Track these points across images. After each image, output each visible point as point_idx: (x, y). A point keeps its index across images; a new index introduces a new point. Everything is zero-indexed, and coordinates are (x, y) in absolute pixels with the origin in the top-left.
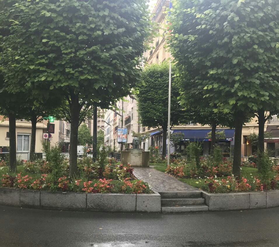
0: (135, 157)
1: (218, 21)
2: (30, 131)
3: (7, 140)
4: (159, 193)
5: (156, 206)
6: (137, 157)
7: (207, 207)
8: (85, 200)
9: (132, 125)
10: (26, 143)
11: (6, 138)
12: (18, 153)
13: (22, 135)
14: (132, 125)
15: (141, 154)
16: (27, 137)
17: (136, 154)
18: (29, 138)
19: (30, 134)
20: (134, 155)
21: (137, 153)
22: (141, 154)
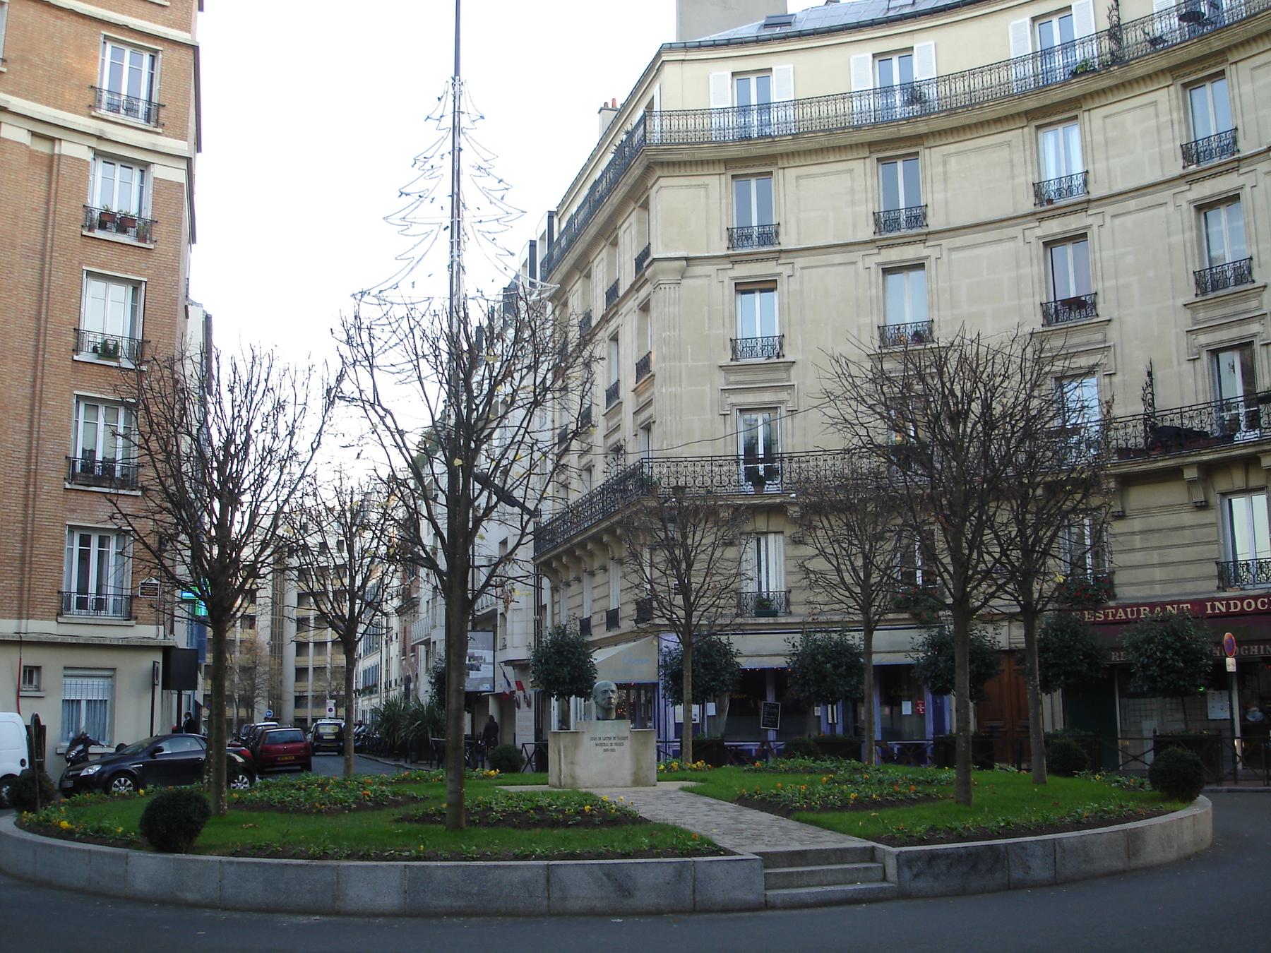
0: (606, 750)
6: (613, 750)
12: (1209, 578)
20: (601, 745)
21: (610, 738)
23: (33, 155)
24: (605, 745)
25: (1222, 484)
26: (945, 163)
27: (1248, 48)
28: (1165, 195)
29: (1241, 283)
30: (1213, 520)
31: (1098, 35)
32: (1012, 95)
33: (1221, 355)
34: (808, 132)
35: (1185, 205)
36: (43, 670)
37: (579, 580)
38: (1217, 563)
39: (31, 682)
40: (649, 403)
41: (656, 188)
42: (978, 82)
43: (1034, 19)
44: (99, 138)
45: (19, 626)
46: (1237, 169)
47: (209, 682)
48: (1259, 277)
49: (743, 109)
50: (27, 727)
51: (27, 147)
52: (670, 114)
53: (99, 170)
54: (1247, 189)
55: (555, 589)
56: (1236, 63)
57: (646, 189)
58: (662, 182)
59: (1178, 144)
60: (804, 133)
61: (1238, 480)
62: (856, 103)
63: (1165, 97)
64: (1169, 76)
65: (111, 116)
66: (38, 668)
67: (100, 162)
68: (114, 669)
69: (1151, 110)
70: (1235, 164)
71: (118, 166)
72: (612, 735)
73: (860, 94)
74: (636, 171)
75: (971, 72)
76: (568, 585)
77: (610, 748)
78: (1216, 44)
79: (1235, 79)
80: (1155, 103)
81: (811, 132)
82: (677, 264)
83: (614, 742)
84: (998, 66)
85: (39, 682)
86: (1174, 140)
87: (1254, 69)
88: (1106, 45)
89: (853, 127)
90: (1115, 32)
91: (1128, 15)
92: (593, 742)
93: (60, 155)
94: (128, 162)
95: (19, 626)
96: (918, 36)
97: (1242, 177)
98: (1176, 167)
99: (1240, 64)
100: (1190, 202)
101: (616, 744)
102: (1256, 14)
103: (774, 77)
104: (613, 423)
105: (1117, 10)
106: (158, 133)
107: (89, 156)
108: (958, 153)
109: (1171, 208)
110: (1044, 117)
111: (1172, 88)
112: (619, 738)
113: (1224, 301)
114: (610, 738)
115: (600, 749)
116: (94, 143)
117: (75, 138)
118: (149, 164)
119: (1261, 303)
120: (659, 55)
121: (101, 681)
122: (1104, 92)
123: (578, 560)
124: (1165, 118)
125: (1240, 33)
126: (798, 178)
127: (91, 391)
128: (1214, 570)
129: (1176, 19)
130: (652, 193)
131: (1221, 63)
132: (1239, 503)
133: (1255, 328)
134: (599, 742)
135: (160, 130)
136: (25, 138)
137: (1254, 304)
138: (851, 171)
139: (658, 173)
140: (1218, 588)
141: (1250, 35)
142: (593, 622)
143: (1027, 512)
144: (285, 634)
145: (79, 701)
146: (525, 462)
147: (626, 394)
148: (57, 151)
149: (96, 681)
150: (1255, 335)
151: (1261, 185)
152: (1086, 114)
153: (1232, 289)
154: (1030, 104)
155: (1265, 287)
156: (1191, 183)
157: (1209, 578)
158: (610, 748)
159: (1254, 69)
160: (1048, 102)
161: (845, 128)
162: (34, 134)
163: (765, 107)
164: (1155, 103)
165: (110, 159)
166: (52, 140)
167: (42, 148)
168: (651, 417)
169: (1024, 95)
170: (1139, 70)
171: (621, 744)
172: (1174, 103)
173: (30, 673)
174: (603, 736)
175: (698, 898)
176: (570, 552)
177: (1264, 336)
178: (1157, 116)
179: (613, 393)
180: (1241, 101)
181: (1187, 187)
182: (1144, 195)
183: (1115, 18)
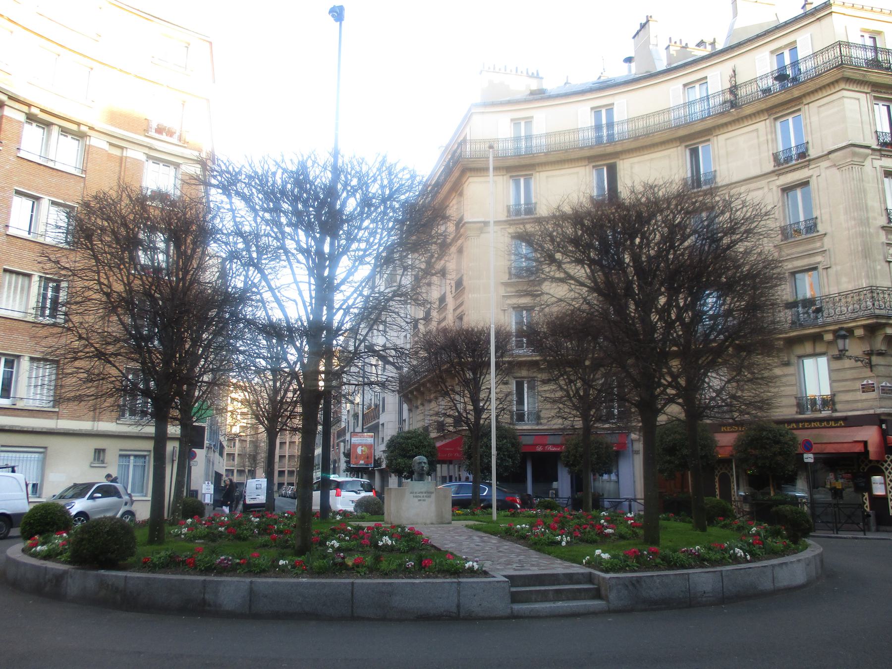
0: (420, 500)
1: (796, 474)
2: (150, 445)
3: (94, 469)
4: (505, 576)
5: (502, 606)
6: (424, 500)
7: (604, 602)
8: (350, 594)
9: (383, 425)
10: (139, 471)
11: (91, 463)
12: (791, 406)
13: (129, 456)
14: (383, 425)
15: (432, 493)
16: (142, 460)
17: (422, 495)
18: (145, 462)
19: (150, 451)
20: (416, 497)
21: (422, 493)
22: (432, 493)
23: (110, 156)
25: (799, 350)
26: (632, 168)
27: (816, 94)
28: (763, 183)
29: (810, 233)
30: (793, 372)
31: (723, 92)
32: (672, 128)
33: (798, 276)
34: (553, 151)
35: (775, 188)
36: (106, 451)
37: (423, 405)
38: (796, 398)
39: (99, 458)
40: (461, 304)
41: (467, 183)
42: (651, 121)
43: (685, 85)
44: (150, 148)
45: (93, 426)
46: (808, 166)
48: (821, 228)
49: (517, 139)
51: (106, 151)
52: (475, 142)
53: (150, 166)
54: (814, 178)
55: (410, 410)
56: (808, 104)
57: (462, 185)
58: (471, 179)
59: (771, 153)
60: (551, 151)
61: (808, 348)
62: (581, 135)
63: (762, 126)
64: (766, 114)
65: (157, 136)
66: (104, 450)
67: (150, 162)
68: (45, 448)
69: (755, 134)
70: (807, 163)
71: (161, 164)
73: (583, 130)
74: (456, 174)
75: (648, 116)
76: (417, 407)
77: (422, 499)
78: (796, 93)
79: (807, 112)
80: (757, 130)
81: (555, 151)
82: (479, 225)
84: (663, 112)
85: (104, 459)
86: (768, 150)
87: (819, 107)
88: (728, 96)
89: (579, 148)
90: (733, 89)
91: (740, 80)
93: (126, 157)
94: (167, 163)
95: (93, 426)
96: (617, 97)
97: (811, 171)
98: (770, 166)
99: (810, 105)
100: (778, 187)
102: (820, 75)
103: (535, 121)
104: (442, 316)
105: (735, 77)
106: (185, 147)
107: (143, 158)
108: (639, 162)
109: (766, 190)
110: (690, 140)
111: (768, 121)
112: (428, 493)
113: (799, 243)
114: (422, 493)
115: (416, 499)
116: (147, 151)
117: (136, 147)
118: (180, 164)
119: (823, 244)
120: (470, 110)
121: (37, 455)
122: (726, 125)
123: (422, 394)
124: (763, 138)
125: (811, 86)
126: (547, 177)
127: (24, 188)
128: (793, 401)
129: (771, 80)
130: (465, 186)
131: (799, 104)
132: (809, 363)
133: (818, 259)
135: (186, 145)
136: (106, 147)
137: (818, 244)
138: (578, 173)
139: (468, 174)
140: (797, 412)
141: (818, 86)
142: (430, 429)
147: (450, 300)
148: (124, 154)
149: (33, 455)
150: (819, 263)
151: (823, 175)
152: (715, 138)
153: (804, 236)
154: (681, 133)
155: (825, 234)
156: (779, 175)
157: (791, 406)
158: (422, 499)
159: (819, 107)
160: (693, 131)
161: (575, 148)
162: (111, 144)
163: (529, 138)
164: (757, 130)
165: (157, 160)
166: (122, 148)
167: (117, 152)
168: (463, 311)
169: (678, 127)
170: (748, 110)
171: (429, 497)
172: (769, 129)
173: (99, 453)
176: (417, 389)
177: (825, 263)
178: (758, 137)
179: (442, 299)
180: (811, 126)
181: (776, 178)
182: (750, 183)
183: (733, 82)
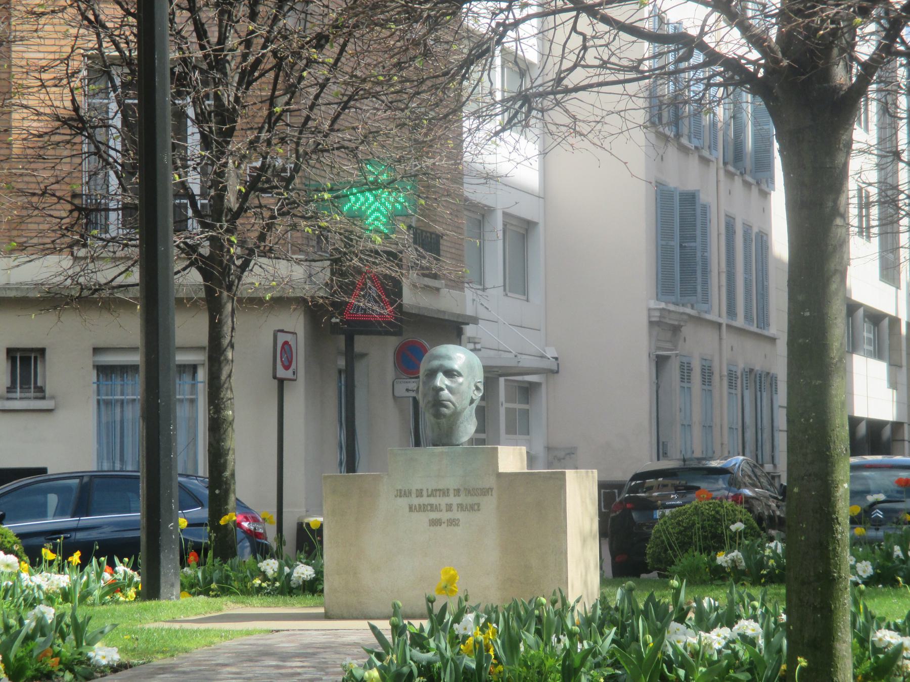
0: (435, 523)
6: (453, 522)
20: (423, 508)
21: (445, 493)
24: (434, 508)
47: (222, 396)
50: (322, 555)
72: (450, 483)
77: (445, 516)
83: (454, 500)
92: (403, 502)
101: (461, 507)
114: (445, 493)
115: (423, 518)
134: (416, 501)
143: (456, 90)
144: (375, 339)
145: (428, 496)
146: (367, 108)
158: (445, 516)
171: (473, 508)
174: (432, 485)
175: (907, 246)
